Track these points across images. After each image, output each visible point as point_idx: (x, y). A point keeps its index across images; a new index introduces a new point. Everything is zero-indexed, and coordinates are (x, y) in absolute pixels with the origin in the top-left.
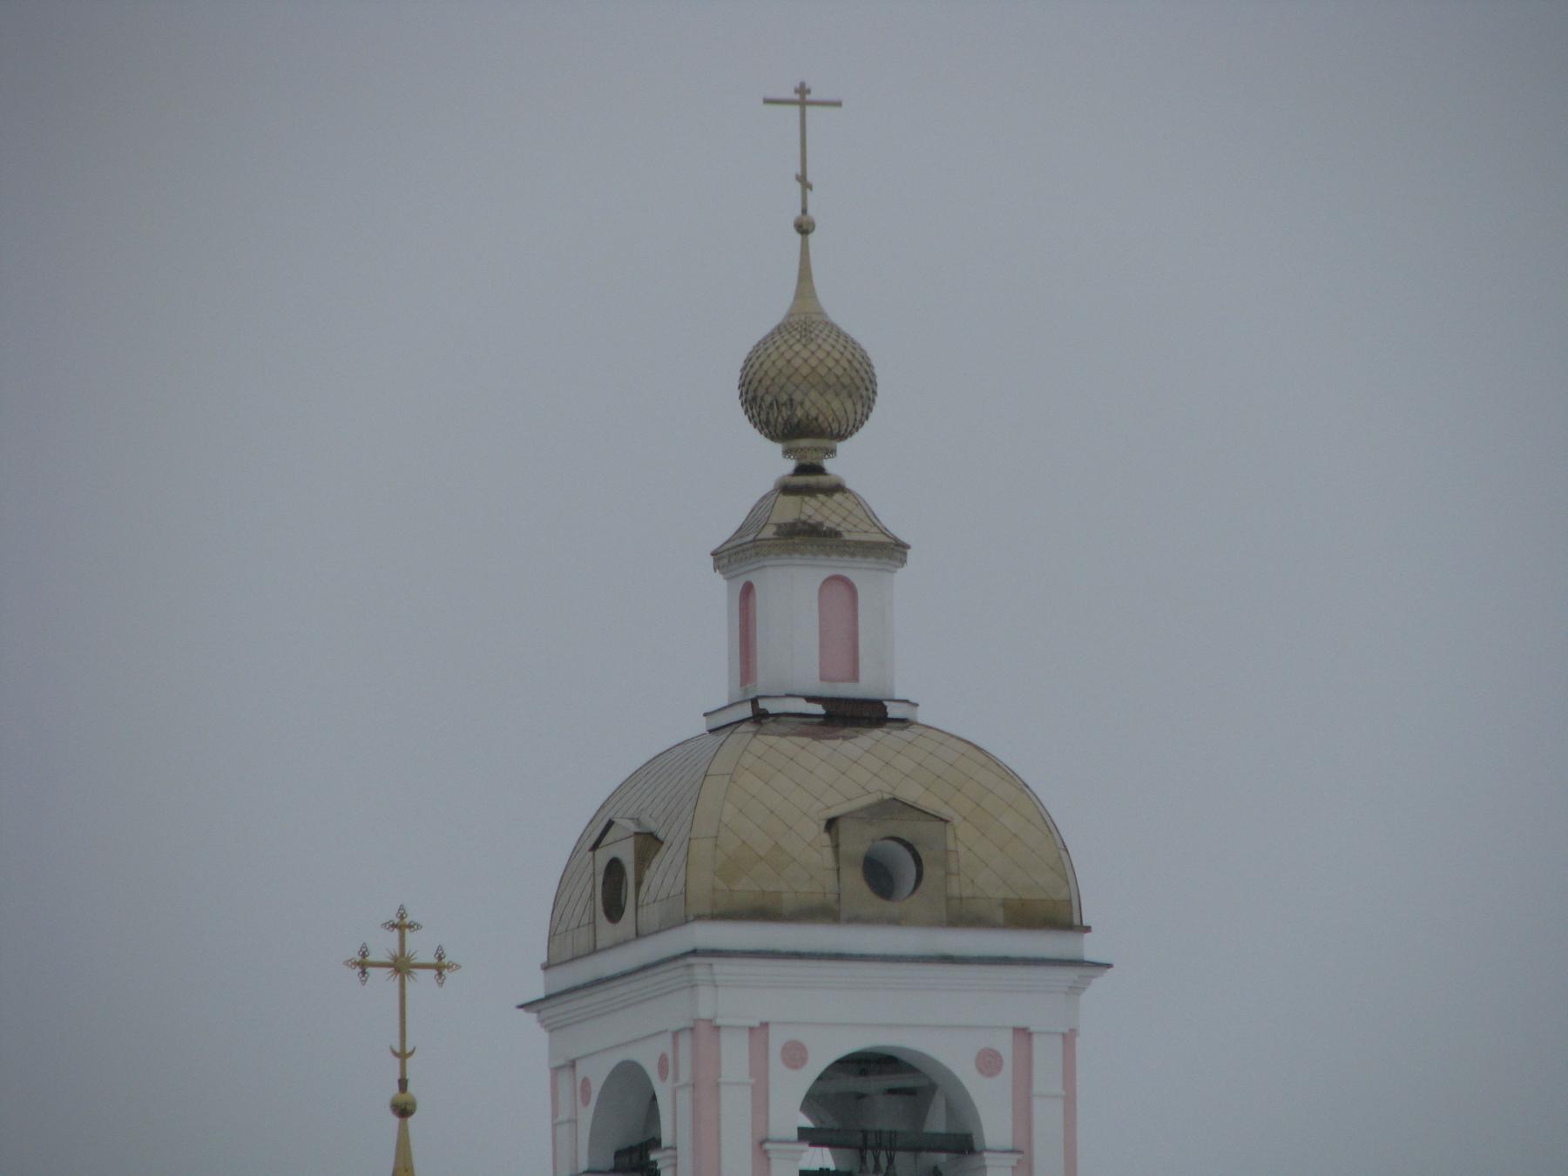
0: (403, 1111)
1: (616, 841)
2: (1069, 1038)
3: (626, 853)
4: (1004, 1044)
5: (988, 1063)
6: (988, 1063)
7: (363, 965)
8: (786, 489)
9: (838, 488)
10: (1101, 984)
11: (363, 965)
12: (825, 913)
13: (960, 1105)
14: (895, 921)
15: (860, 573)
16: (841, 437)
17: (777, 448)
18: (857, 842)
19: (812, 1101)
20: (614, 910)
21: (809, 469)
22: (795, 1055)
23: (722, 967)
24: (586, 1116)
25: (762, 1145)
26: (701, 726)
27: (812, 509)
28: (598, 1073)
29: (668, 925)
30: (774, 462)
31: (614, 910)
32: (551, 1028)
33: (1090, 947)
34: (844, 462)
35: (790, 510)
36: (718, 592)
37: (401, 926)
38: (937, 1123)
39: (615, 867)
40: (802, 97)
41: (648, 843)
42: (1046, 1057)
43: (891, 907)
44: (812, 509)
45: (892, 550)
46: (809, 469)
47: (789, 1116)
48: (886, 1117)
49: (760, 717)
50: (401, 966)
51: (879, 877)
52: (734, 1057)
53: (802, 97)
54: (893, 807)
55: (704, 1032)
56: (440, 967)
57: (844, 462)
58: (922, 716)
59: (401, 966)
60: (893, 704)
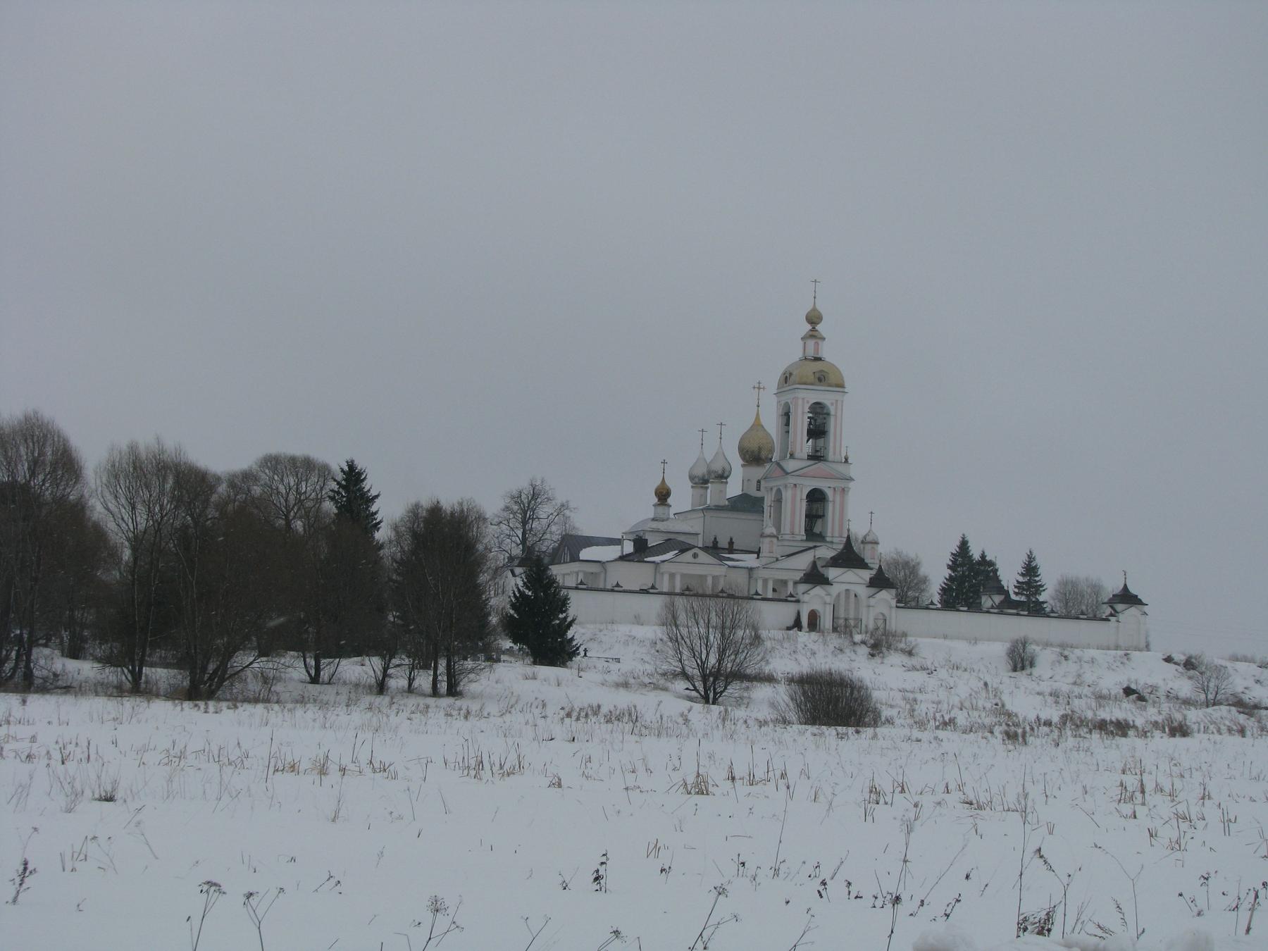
0: (758, 406)
1: (834, 462)
2: (842, 401)
3: (788, 376)
4: (834, 402)
5: (832, 404)
6: (832, 404)
7: (754, 388)
8: (811, 330)
9: (817, 331)
10: (847, 395)
11: (754, 388)
12: (812, 384)
13: (828, 409)
14: (822, 385)
15: (820, 342)
16: (818, 324)
17: (809, 325)
18: (817, 375)
19: (810, 408)
20: (786, 383)
21: (814, 329)
22: (808, 402)
23: (799, 390)
24: (782, 408)
25: (803, 413)
26: (798, 360)
27: (814, 333)
28: (783, 403)
29: (793, 384)
30: (809, 327)
31: (786, 383)
32: (777, 397)
33: (846, 390)
34: (818, 327)
35: (811, 333)
36: (801, 343)
37: (764, 388)
38: (825, 411)
39: (786, 377)
40: (815, 281)
41: (791, 374)
42: (839, 403)
43: (822, 384)
44: (814, 333)
45: (824, 339)
46: (814, 329)
47: (807, 409)
48: (819, 410)
49: (806, 359)
50: (759, 388)
51: (820, 380)
52: (800, 402)
53: (815, 281)
54: (822, 371)
55: (797, 398)
56: (764, 388)
57: (818, 327)
58: (827, 360)
59: (759, 388)
60: (810, 588)
